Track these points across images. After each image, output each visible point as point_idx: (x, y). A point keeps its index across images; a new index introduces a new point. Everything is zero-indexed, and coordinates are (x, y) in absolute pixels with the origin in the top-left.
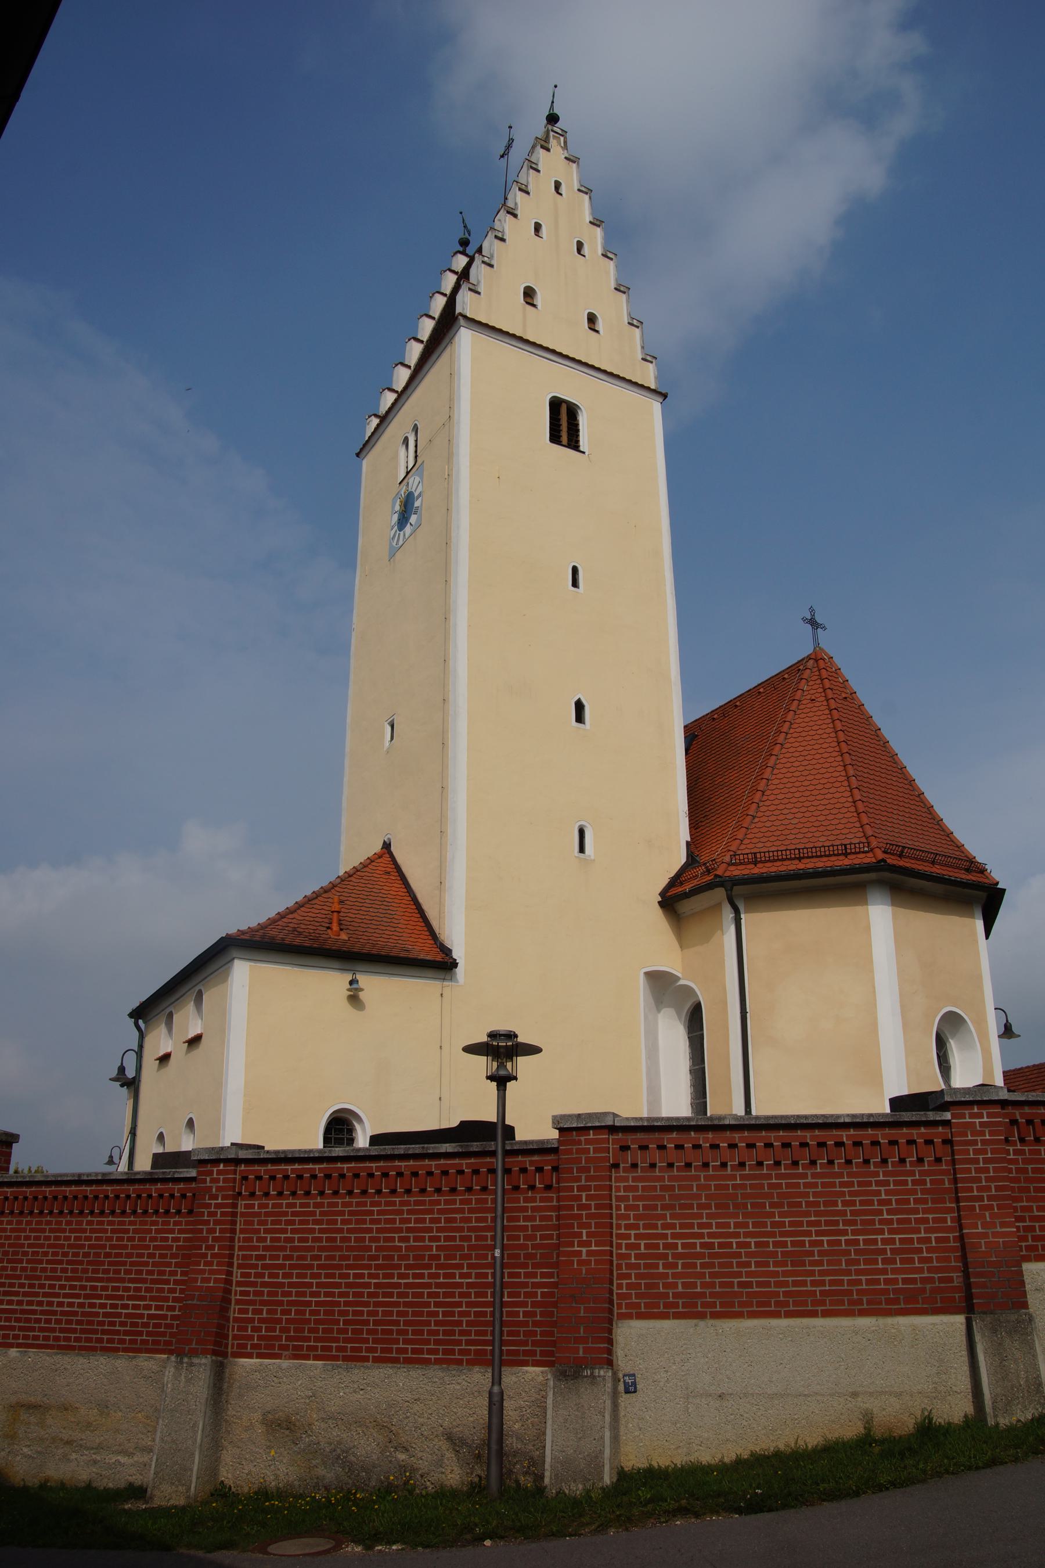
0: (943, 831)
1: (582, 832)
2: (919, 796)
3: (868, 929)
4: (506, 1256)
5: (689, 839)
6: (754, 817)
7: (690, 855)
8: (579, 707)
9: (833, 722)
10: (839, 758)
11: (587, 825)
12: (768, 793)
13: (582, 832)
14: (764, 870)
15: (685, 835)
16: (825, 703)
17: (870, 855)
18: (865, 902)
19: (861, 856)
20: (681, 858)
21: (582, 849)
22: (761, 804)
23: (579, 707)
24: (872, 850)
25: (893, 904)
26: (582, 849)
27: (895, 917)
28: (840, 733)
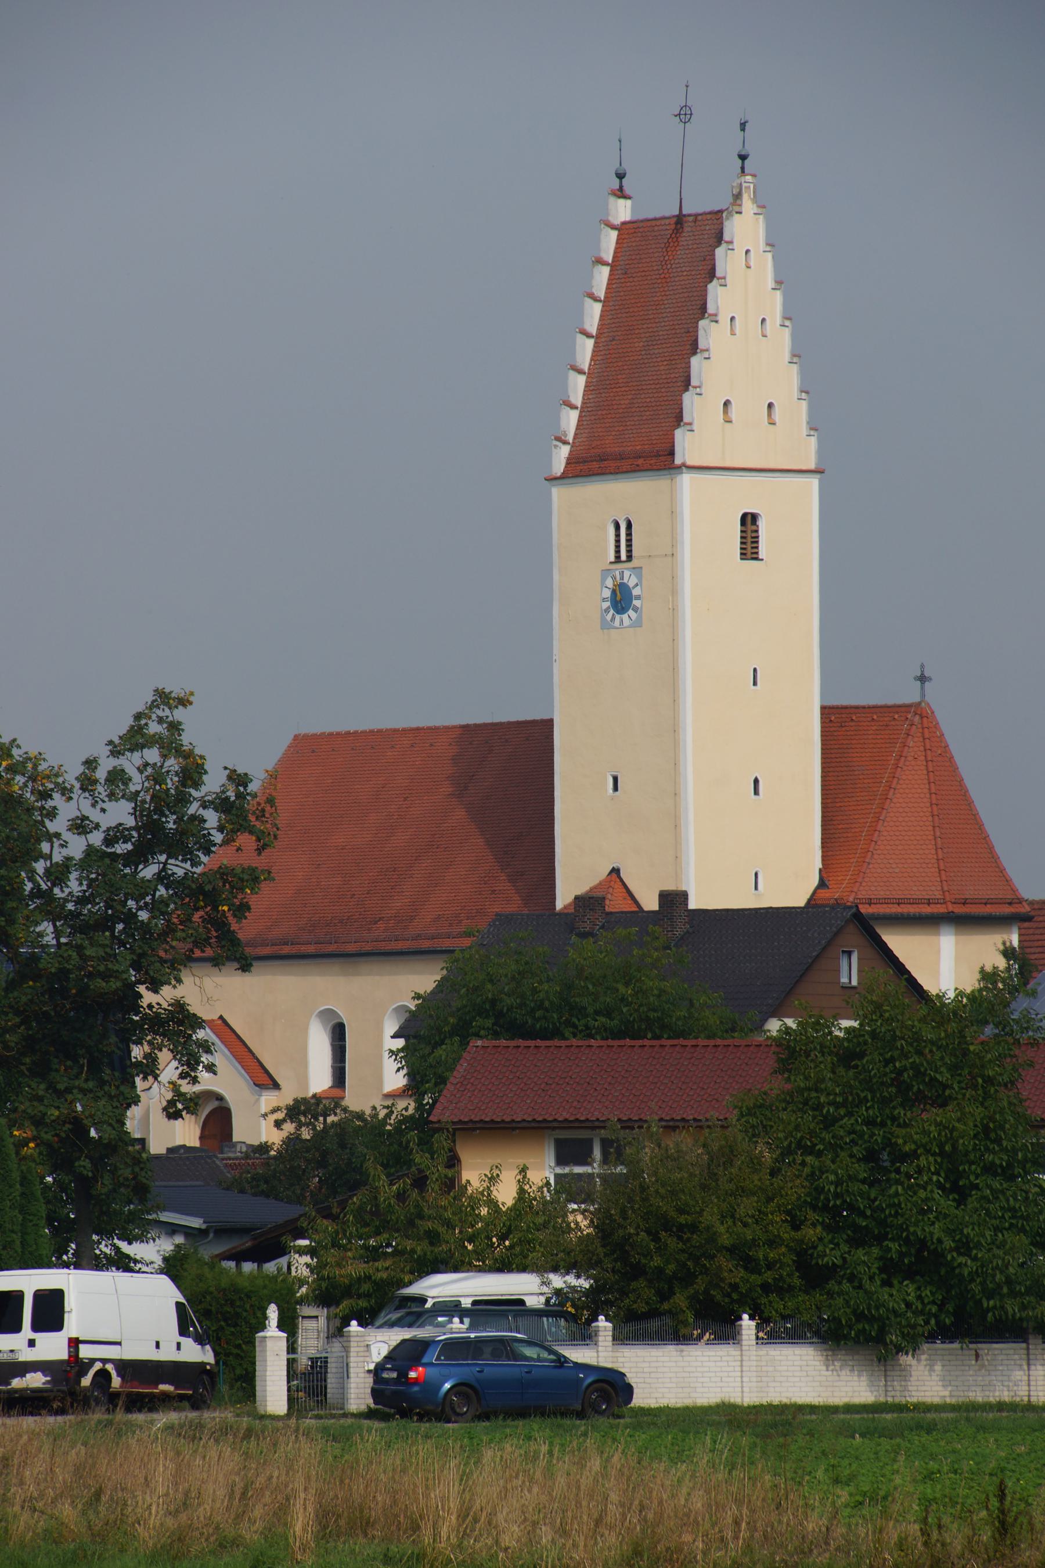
0: (998, 867)
1: (756, 874)
2: (985, 838)
3: (939, 952)
4: (748, 184)
5: (821, 866)
6: (869, 863)
7: (821, 879)
8: (749, 548)
9: (925, 750)
10: (930, 819)
11: (763, 518)
12: (864, 884)
13: (756, 874)
14: (875, 910)
15: (819, 864)
16: (925, 763)
17: (944, 906)
18: (939, 934)
19: (938, 906)
20: (815, 881)
21: (756, 888)
22: (875, 852)
23: (749, 548)
24: (945, 903)
25: (956, 934)
26: (756, 888)
27: (957, 943)
28: (934, 795)
